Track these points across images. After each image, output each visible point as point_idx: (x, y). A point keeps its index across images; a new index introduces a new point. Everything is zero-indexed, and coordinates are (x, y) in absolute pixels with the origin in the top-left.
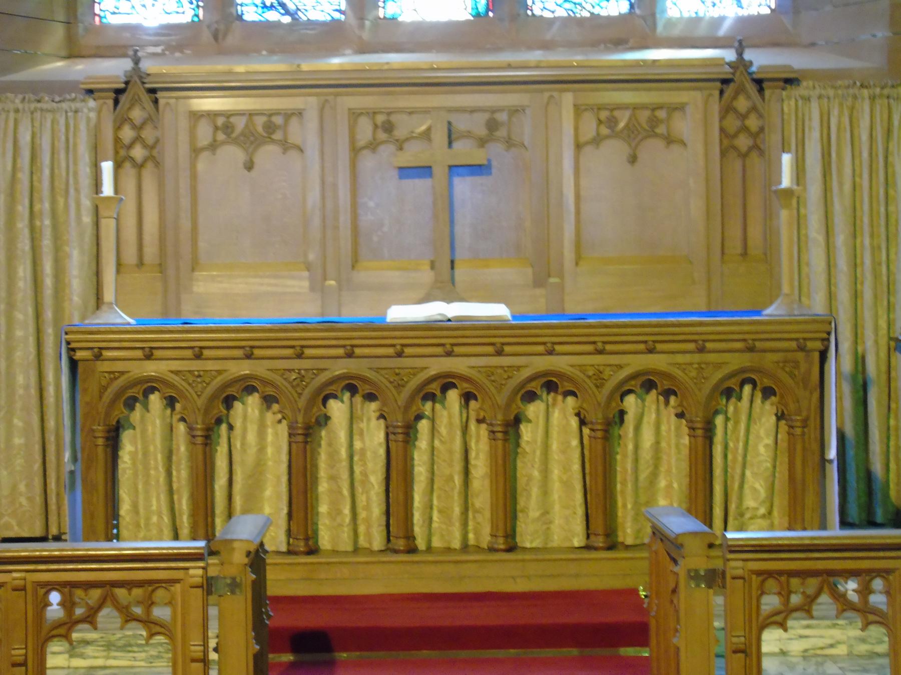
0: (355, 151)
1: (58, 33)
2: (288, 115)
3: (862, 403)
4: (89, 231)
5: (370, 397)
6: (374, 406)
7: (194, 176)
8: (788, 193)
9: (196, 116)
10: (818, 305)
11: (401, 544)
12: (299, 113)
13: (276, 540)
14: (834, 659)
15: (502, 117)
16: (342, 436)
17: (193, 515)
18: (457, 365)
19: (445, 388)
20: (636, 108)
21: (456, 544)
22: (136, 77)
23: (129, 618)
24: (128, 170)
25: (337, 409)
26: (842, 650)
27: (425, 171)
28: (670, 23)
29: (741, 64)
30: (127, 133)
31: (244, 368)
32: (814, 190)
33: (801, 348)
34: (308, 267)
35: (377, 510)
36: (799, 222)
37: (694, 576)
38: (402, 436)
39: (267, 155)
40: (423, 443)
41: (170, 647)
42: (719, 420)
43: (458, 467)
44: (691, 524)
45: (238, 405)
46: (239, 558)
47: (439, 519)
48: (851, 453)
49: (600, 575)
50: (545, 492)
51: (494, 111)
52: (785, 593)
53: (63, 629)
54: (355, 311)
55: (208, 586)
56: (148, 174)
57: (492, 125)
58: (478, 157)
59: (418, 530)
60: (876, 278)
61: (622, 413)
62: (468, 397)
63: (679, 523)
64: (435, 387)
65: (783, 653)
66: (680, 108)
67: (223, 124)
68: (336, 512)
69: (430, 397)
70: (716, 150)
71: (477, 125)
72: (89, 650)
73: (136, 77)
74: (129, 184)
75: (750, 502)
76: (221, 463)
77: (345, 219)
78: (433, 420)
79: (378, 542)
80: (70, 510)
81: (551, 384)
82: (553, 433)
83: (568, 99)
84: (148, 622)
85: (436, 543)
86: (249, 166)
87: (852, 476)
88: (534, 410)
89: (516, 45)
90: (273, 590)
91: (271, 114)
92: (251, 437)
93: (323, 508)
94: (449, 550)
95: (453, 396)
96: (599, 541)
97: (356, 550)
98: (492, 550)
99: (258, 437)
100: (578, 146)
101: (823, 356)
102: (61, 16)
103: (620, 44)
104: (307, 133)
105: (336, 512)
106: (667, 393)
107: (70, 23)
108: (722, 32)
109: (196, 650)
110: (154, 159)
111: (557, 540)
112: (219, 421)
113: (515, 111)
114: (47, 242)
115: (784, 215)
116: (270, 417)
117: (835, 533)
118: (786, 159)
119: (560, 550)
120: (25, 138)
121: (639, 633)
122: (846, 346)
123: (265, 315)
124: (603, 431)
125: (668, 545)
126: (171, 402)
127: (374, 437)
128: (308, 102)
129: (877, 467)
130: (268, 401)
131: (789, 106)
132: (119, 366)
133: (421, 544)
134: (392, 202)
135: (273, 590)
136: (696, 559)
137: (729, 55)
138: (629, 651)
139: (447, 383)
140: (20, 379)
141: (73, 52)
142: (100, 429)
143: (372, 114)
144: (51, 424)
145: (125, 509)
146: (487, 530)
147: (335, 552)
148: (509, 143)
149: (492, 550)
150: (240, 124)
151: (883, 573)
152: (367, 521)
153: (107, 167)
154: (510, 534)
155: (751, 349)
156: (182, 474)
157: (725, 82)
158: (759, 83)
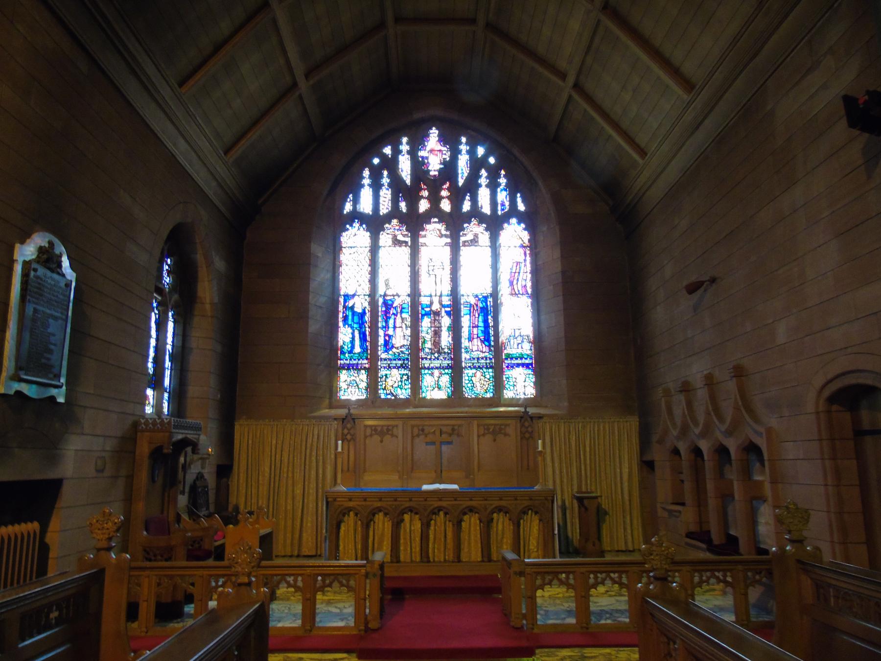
0: (413, 437)
1: (327, 401)
2: (393, 426)
3: (564, 514)
4: (333, 460)
5: (416, 513)
6: (417, 516)
7: (365, 444)
8: (541, 452)
9: (366, 426)
10: (550, 486)
11: (425, 560)
12: (397, 426)
13: (388, 558)
14: (559, 598)
15: (456, 427)
16: (408, 525)
17: (362, 550)
18: (444, 504)
19: (439, 511)
20: (495, 425)
21: (442, 560)
22: (349, 415)
23: (342, 585)
24: (346, 443)
25: (407, 517)
26: (561, 595)
27: (433, 443)
28: (505, 399)
29: (526, 412)
30: (346, 431)
31: (379, 504)
32: (548, 450)
33: (546, 499)
34: (398, 472)
35: (418, 549)
36: (544, 460)
37: (516, 573)
38: (426, 525)
39: (387, 438)
40: (432, 528)
41: (449, 240)
42: (522, 521)
43: (443, 535)
44: (516, 557)
45: (377, 516)
46: (376, 566)
47: (437, 552)
48: (562, 530)
49: (486, 570)
50: (469, 544)
51: (453, 425)
52: (543, 579)
53: (322, 589)
54: (412, 486)
55: (367, 576)
56: (352, 443)
57: (453, 430)
58: (449, 439)
59: (431, 555)
60: (699, 506)
61: (492, 519)
62: (446, 514)
63: (510, 556)
64: (436, 511)
65: (543, 596)
66: (508, 425)
67: (374, 429)
68: (406, 550)
69: (434, 513)
70: (519, 438)
71: (449, 430)
72: (329, 594)
73: (349, 415)
74: (346, 447)
75: (531, 547)
76: (371, 533)
77: (409, 458)
78: (435, 520)
79: (418, 559)
80: (325, 548)
81: (471, 510)
82: (472, 525)
83: (475, 422)
84: (348, 586)
85: (436, 559)
86: (382, 441)
87: (562, 538)
88: (466, 517)
89: (461, 406)
90: (387, 574)
91: (388, 426)
92: (381, 526)
93: (402, 548)
94: (440, 562)
95: (442, 513)
96: (486, 559)
97: (412, 561)
98: (453, 562)
99: (382, 525)
100: (479, 436)
101: (553, 502)
102: (328, 396)
103: (491, 406)
104: (399, 432)
105: (406, 550)
106: (506, 513)
107: (331, 398)
108: (520, 402)
109: (362, 596)
110: (353, 439)
111: (473, 558)
112: (371, 520)
113: (459, 426)
114: (321, 463)
115: (540, 459)
116: (386, 519)
117: (558, 559)
118: (540, 441)
119: (474, 562)
120: (316, 432)
121: (498, 590)
122: (559, 497)
123: (384, 487)
124: (487, 524)
125: (508, 563)
126: (356, 515)
127: (418, 525)
128: (400, 423)
129: (570, 534)
130: (386, 514)
131: (540, 425)
132: (340, 503)
133: (431, 560)
134: (423, 451)
135: (387, 574)
136: (516, 568)
137: (522, 409)
138: (496, 596)
139: (440, 509)
140: (311, 506)
141: (331, 407)
142: (335, 522)
143: (418, 426)
144: (319, 519)
145: (341, 548)
146: (452, 555)
147: (405, 562)
148: (458, 435)
149: (453, 562)
150: (379, 429)
151: (573, 572)
152: (415, 553)
153: (340, 442)
154: (459, 557)
155: (531, 499)
156: (359, 537)
157: (522, 417)
158: (531, 418)
